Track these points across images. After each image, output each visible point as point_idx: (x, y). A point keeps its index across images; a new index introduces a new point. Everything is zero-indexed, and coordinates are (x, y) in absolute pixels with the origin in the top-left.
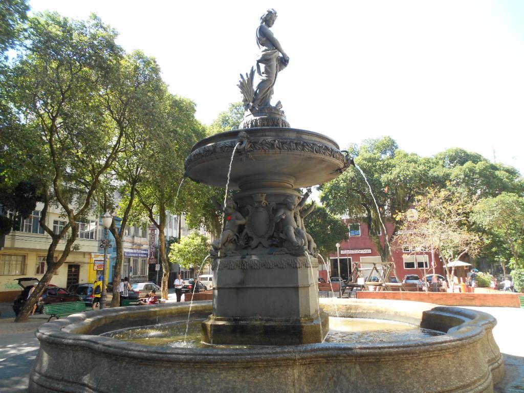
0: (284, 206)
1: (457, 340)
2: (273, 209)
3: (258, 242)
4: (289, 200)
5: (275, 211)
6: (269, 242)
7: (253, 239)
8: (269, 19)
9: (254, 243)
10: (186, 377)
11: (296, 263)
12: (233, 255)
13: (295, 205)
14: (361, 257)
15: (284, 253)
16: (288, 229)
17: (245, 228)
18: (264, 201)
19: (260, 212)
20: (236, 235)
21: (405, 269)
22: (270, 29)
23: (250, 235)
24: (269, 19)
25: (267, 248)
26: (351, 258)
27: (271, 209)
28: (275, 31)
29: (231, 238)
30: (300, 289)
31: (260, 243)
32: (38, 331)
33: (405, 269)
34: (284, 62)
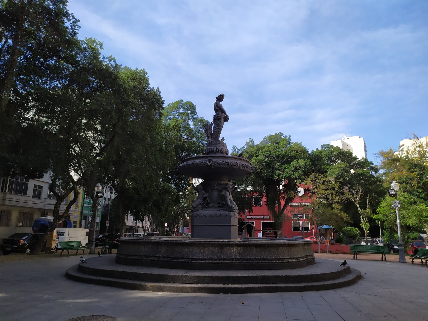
0: (225, 189)
1: (166, 257)
2: (220, 190)
3: (212, 205)
4: (227, 187)
5: (221, 191)
6: (218, 205)
7: (210, 204)
8: (220, 98)
9: (211, 205)
10: (259, 158)
11: (230, 215)
12: (201, 210)
13: (230, 189)
14: (269, 218)
15: (225, 210)
16: (227, 200)
17: (207, 198)
18: (216, 186)
19: (214, 191)
20: (203, 202)
21: (293, 231)
22: (221, 103)
23: (209, 202)
24: (220, 98)
25: (217, 208)
26: (254, 221)
27: (219, 190)
28: (224, 104)
29: (201, 203)
30: (232, 227)
31: (214, 205)
32: (18, 84)
33: (293, 231)
34: (226, 119)
